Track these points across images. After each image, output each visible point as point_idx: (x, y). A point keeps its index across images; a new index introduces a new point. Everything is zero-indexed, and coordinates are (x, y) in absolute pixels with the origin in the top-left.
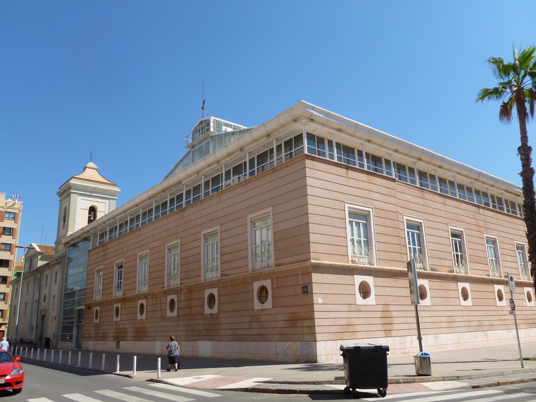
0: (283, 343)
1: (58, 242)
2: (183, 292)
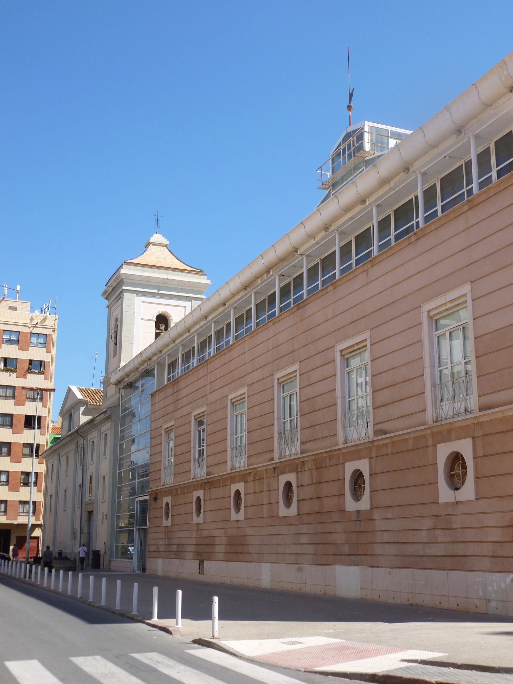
0: (498, 575)
1: (106, 382)
2: (306, 468)
